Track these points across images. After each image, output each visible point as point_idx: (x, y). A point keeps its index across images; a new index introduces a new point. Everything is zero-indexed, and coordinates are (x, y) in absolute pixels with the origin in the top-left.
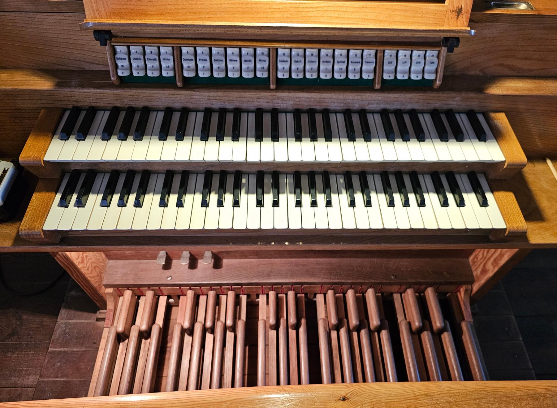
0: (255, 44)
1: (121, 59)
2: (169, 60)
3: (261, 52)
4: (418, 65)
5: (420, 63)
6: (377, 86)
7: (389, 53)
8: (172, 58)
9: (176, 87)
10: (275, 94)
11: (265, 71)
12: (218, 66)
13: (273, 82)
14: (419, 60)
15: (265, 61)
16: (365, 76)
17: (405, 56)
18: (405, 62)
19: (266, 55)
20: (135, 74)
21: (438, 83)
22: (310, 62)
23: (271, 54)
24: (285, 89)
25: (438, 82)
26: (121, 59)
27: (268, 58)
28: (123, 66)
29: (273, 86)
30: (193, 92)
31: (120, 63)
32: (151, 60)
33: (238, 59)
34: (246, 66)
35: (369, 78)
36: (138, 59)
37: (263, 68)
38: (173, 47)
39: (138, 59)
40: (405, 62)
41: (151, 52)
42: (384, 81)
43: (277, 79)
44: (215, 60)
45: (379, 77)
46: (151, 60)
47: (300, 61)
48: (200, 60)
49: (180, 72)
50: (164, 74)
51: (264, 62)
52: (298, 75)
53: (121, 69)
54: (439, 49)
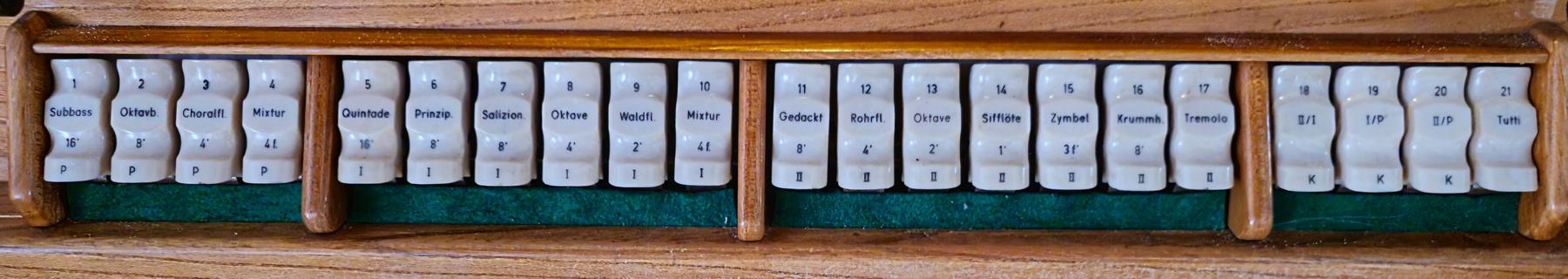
0: (831, 51)
1: (69, 112)
2: (279, 114)
3: (698, 79)
4: (1444, 128)
5: (1449, 119)
6: (1257, 223)
7: (1296, 81)
8: (293, 107)
9: (296, 231)
10: (761, 263)
11: (715, 159)
12: (498, 139)
13: (750, 207)
14: (1442, 108)
15: (715, 117)
16: (1188, 178)
17: (1306, 90)
18: (1380, 118)
19: (721, 95)
20: (485, 176)
21: (1554, 209)
22: (921, 118)
23: (744, 84)
24: (811, 242)
25: (1552, 206)
26: (69, 112)
27: (729, 106)
28: (365, 144)
29: (749, 225)
30: (376, 256)
31: (60, 131)
32: (200, 114)
33: (660, 111)
34: (630, 140)
35: (1212, 187)
36: (141, 113)
37: (703, 147)
38: (736, 64)
39: (141, 113)
40: (1380, 118)
41: (368, 84)
42: (1284, 201)
43: (1278, 191)
44: (489, 115)
45: (1260, 182)
46: (200, 114)
47: (879, 117)
48: (418, 113)
49: (325, 167)
50: (983, 179)
51: (272, 119)
52: (867, 176)
53: (354, 157)
54: (1533, 59)
